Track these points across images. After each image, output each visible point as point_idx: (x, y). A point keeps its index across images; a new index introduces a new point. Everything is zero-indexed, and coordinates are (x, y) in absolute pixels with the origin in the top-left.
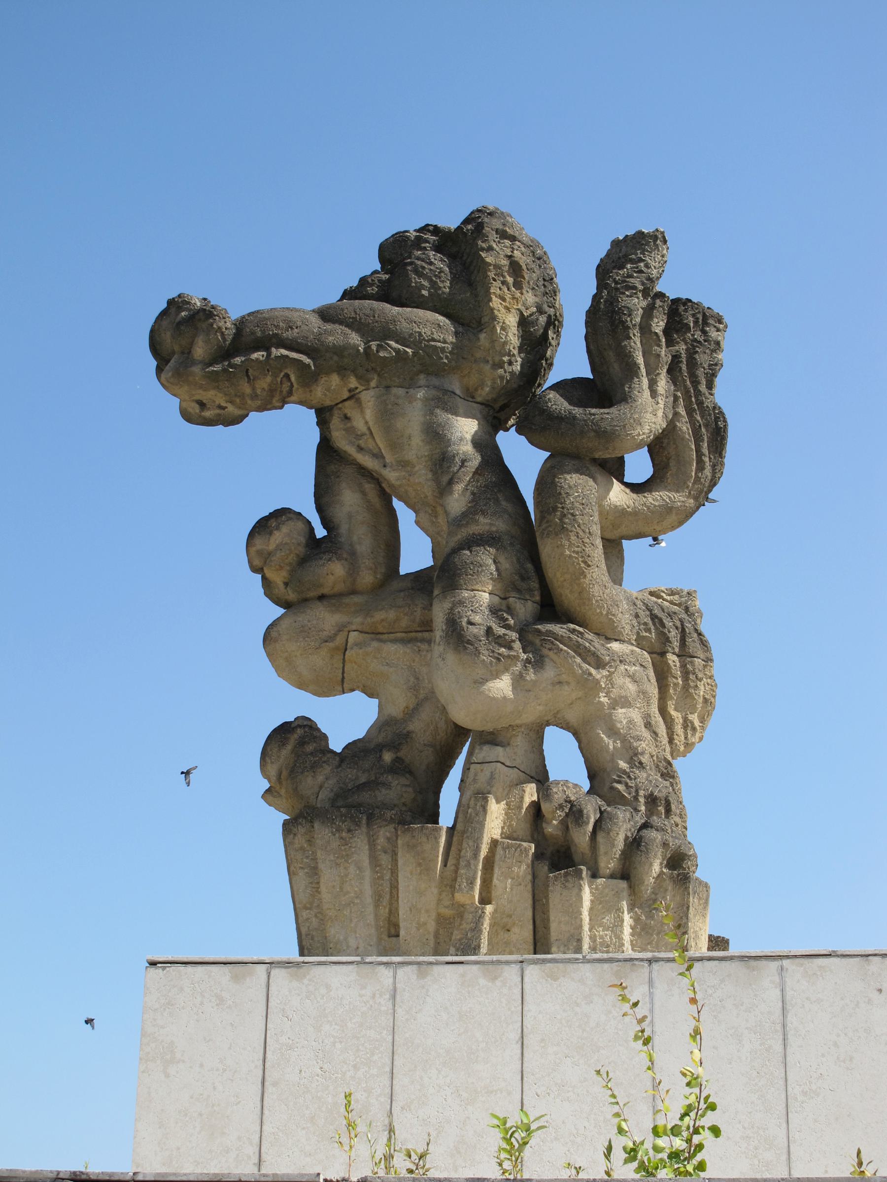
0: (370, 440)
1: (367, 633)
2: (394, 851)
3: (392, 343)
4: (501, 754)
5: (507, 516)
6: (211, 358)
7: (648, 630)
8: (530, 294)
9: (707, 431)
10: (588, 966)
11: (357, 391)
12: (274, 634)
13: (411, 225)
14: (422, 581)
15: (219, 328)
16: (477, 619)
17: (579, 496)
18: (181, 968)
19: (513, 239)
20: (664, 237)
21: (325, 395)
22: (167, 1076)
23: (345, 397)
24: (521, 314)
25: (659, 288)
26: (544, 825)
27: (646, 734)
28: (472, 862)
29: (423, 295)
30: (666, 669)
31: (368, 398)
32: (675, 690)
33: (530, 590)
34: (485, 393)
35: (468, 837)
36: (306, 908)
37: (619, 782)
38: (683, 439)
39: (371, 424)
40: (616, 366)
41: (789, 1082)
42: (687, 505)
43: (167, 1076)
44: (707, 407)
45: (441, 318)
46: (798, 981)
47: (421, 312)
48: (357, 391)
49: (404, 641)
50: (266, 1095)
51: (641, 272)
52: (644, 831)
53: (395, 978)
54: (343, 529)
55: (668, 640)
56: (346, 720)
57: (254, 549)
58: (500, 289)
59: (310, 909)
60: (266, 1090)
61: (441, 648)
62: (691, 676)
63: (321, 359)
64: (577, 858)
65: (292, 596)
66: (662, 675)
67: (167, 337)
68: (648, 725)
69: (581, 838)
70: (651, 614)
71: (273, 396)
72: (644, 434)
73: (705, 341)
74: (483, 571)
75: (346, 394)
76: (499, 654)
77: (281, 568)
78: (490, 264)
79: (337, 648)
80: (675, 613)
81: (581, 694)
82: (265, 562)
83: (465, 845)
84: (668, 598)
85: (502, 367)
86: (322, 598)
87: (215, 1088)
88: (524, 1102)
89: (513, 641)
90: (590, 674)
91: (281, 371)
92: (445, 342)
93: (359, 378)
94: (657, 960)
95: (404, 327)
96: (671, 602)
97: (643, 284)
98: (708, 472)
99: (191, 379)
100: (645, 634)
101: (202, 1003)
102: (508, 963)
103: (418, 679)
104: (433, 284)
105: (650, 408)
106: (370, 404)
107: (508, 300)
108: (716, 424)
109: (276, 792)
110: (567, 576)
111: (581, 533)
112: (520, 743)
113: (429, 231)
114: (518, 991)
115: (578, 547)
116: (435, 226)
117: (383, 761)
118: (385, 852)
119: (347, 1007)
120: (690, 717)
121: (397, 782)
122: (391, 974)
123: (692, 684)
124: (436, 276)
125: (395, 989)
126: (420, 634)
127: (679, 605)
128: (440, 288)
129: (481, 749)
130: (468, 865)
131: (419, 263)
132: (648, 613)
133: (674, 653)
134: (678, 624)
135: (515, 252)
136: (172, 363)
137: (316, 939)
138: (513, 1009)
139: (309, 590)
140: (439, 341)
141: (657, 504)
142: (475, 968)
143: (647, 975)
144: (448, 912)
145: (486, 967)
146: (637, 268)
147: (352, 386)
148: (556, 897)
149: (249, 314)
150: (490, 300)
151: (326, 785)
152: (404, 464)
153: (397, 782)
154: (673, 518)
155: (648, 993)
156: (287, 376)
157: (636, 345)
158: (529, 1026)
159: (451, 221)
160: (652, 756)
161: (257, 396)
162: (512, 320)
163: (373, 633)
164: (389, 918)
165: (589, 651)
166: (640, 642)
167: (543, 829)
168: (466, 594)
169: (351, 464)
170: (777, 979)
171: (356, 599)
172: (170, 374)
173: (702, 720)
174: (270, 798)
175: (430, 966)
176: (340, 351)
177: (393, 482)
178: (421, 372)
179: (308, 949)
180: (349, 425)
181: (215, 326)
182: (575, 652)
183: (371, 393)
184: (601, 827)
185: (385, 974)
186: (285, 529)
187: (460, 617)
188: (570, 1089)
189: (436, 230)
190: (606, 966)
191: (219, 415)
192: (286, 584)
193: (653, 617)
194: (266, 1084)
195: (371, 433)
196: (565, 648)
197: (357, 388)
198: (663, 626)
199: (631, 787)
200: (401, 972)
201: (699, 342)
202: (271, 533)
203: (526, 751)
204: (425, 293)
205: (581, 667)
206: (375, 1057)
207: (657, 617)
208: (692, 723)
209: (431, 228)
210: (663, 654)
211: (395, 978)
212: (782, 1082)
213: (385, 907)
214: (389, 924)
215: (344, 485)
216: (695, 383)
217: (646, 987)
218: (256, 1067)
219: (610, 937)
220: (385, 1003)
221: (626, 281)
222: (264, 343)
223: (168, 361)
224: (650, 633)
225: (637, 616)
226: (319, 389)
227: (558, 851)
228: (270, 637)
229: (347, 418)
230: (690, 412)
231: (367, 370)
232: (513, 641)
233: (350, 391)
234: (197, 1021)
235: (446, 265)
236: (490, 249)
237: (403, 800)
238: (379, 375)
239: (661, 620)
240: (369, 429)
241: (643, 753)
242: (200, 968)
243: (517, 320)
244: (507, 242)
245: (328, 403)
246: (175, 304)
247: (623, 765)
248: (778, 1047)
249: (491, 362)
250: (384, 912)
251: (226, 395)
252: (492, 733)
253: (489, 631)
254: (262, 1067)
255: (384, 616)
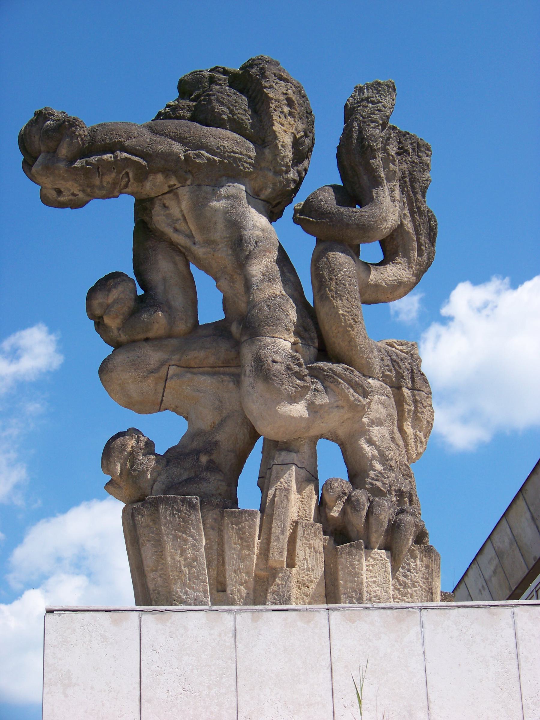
0: (183, 224)
1: (183, 367)
2: (219, 528)
3: (203, 152)
4: (296, 458)
5: (291, 284)
6: (60, 154)
7: (390, 371)
8: (300, 123)
9: (424, 227)
10: (376, 612)
11: (176, 187)
12: (110, 366)
13: (205, 67)
14: (219, 330)
15: (80, 135)
16: (278, 358)
17: (347, 271)
18: (73, 614)
19: (286, 80)
20: (394, 86)
21: (152, 189)
22: (66, 696)
23: (166, 191)
24: (295, 136)
25: (390, 124)
26: (327, 510)
27: (393, 446)
28: (281, 537)
29: (223, 119)
30: (402, 399)
31: (184, 193)
32: (408, 414)
33: (312, 339)
34: (267, 192)
35: (276, 519)
36: (153, 571)
37: (377, 480)
38: (408, 233)
39: (185, 212)
40: (365, 177)
41: (523, 696)
42: (411, 280)
43: (66, 696)
44: (424, 210)
45: (237, 136)
46: (526, 623)
47: (224, 131)
48: (176, 187)
49: (213, 374)
50: (143, 709)
51: (379, 110)
52: (401, 515)
53: (235, 621)
54: (160, 289)
55: (402, 377)
56: (167, 431)
57: (97, 302)
58: (280, 117)
59: (156, 571)
60: (142, 705)
61: (251, 380)
62: (419, 405)
63: (154, 163)
64: (353, 535)
65: (123, 338)
66: (400, 401)
67: (36, 141)
68: (393, 439)
69: (358, 521)
70: (391, 359)
71: (115, 188)
72: (388, 228)
73: (420, 163)
74: (280, 323)
75: (166, 189)
76: (297, 385)
77: (117, 317)
78: (272, 99)
79: (160, 378)
80: (406, 358)
81: (350, 415)
82: (105, 312)
83: (274, 524)
84: (399, 348)
85: (281, 175)
86: (147, 340)
87: (103, 705)
88: (335, 712)
89: (306, 376)
90: (360, 401)
91: (124, 169)
92: (241, 154)
93: (179, 178)
94: (425, 608)
95: (211, 141)
96: (401, 351)
97: (382, 119)
98: (425, 257)
99: (57, 172)
100: (388, 373)
101: (90, 641)
102: (319, 610)
103: (221, 402)
104: (231, 111)
105: (389, 208)
106: (185, 197)
107: (286, 126)
108: (430, 223)
109: (116, 484)
110: (340, 329)
111: (350, 298)
112: (306, 449)
113: (219, 72)
114: (326, 631)
115: (348, 308)
116: (223, 68)
117: (200, 462)
118: (213, 529)
119: (200, 643)
120: (418, 434)
121: (214, 478)
122: (233, 618)
123: (420, 410)
124: (232, 105)
125: (235, 630)
126: (222, 369)
127: (407, 353)
128: (236, 114)
129: (280, 454)
130: (278, 539)
131: (219, 94)
132: (389, 358)
133: (407, 388)
134: (409, 367)
135: (289, 91)
136: (40, 159)
137: (161, 593)
138: (323, 644)
139: (139, 333)
140: (237, 153)
141: (391, 279)
142: (294, 613)
143: (419, 618)
144: (263, 574)
145: (302, 613)
146: (377, 107)
147: (172, 183)
148: (343, 559)
149: (99, 126)
150: (273, 124)
151: (159, 479)
152: (209, 242)
153: (214, 478)
154: (401, 290)
155: (420, 632)
156: (127, 174)
157: (377, 162)
158: (240, 667)
159: (235, 67)
160: (397, 462)
161: (103, 187)
162: (288, 140)
163: (187, 367)
164: (217, 578)
165: (358, 384)
166: (385, 379)
167: (326, 514)
168: (269, 340)
169: (164, 241)
170: (511, 622)
171: (174, 342)
172: (40, 167)
173: (426, 436)
174: (112, 489)
175: (260, 613)
176: (168, 156)
177: (201, 256)
178: (224, 176)
179: (155, 601)
180: (168, 212)
181: (77, 133)
182: (348, 384)
183: (187, 189)
184: (372, 512)
185: (228, 618)
186: (120, 288)
187: (266, 357)
188: (368, 702)
189: (225, 72)
190: (389, 612)
191: (71, 200)
192: (119, 329)
193: (393, 361)
194: (143, 701)
195: (185, 219)
196: (342, 381)
197: (175, 185)
198: (400, 367)
199: (386, 484)
200: (239, 617)
201: (416, 164)
202: (109, 291)
203: (309, 456)
204: (224, 117)
205: (353, 396)
206: (224, 680)
207: (395, 361)
208: (420, 438)
209: (221, 70)
210: (399, 388)
211: (235, 621)
212: (518, 696)
213: (214, 570)
214: (217, 582)
215: (160, 257)
216: (415, 193)
217: (419, 628)
218: (134, 688)
219: (381, 592)
220: (229, 640)
221: (370, 117)
222: (111, 149)
223: (36, 158)
224: (391, 372)
225: (382, 360)
226: (148, 184)
227: (336, 530)
228: (104, 369)
229: (165, 206)
230: (412, 213)
231: (186, 172)
232: (306, 376)
233: (169, 187)
234: (88, 654)
235: (233, 96)
236: (271, 87)
237: (219, 491)
238: (193, 176)
239: (398, 363)
240: (183, 215)
241: (391, 460)
242: (87, 614)
243: (292, 140)
244: (283, 83)
245: (153, 195)
246: (41, 116)
247: (378, 466)
248: (514, 670)
249: (273, 170)
250: (214, 573)
251: (80, 185)
252: (286, 443)
253: (288, 368)
254: (139, 688)
255: (196, 355)
